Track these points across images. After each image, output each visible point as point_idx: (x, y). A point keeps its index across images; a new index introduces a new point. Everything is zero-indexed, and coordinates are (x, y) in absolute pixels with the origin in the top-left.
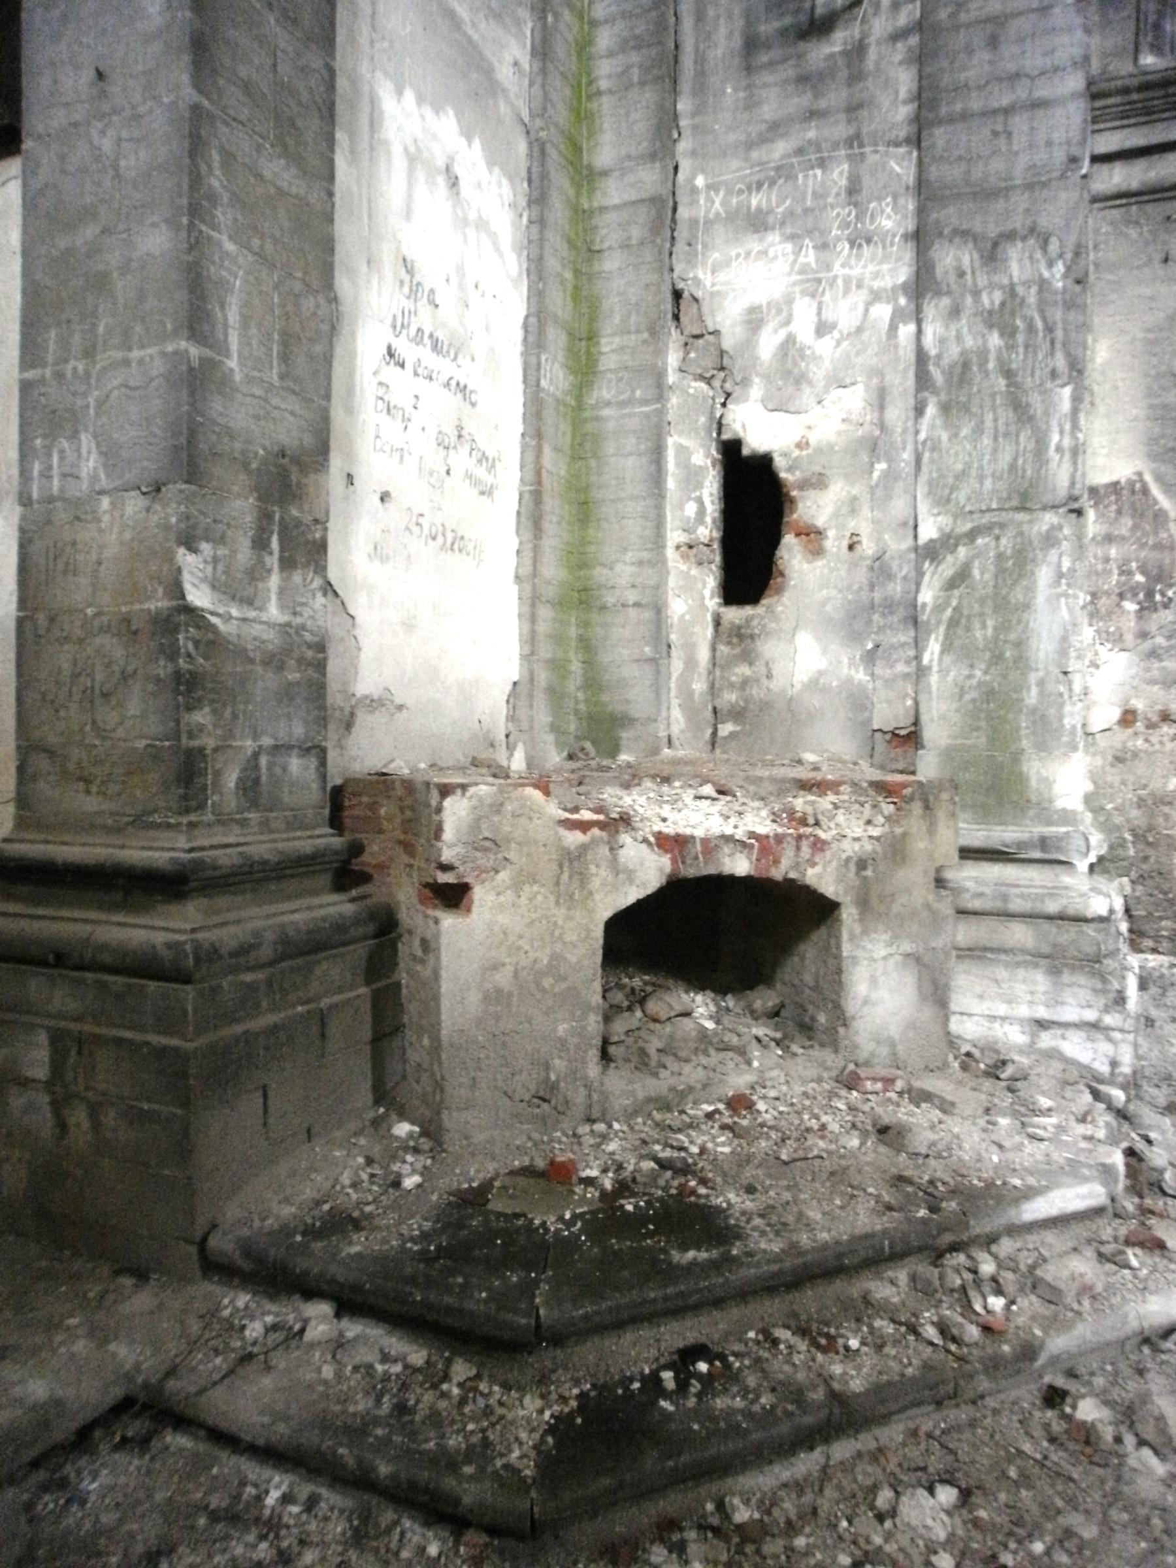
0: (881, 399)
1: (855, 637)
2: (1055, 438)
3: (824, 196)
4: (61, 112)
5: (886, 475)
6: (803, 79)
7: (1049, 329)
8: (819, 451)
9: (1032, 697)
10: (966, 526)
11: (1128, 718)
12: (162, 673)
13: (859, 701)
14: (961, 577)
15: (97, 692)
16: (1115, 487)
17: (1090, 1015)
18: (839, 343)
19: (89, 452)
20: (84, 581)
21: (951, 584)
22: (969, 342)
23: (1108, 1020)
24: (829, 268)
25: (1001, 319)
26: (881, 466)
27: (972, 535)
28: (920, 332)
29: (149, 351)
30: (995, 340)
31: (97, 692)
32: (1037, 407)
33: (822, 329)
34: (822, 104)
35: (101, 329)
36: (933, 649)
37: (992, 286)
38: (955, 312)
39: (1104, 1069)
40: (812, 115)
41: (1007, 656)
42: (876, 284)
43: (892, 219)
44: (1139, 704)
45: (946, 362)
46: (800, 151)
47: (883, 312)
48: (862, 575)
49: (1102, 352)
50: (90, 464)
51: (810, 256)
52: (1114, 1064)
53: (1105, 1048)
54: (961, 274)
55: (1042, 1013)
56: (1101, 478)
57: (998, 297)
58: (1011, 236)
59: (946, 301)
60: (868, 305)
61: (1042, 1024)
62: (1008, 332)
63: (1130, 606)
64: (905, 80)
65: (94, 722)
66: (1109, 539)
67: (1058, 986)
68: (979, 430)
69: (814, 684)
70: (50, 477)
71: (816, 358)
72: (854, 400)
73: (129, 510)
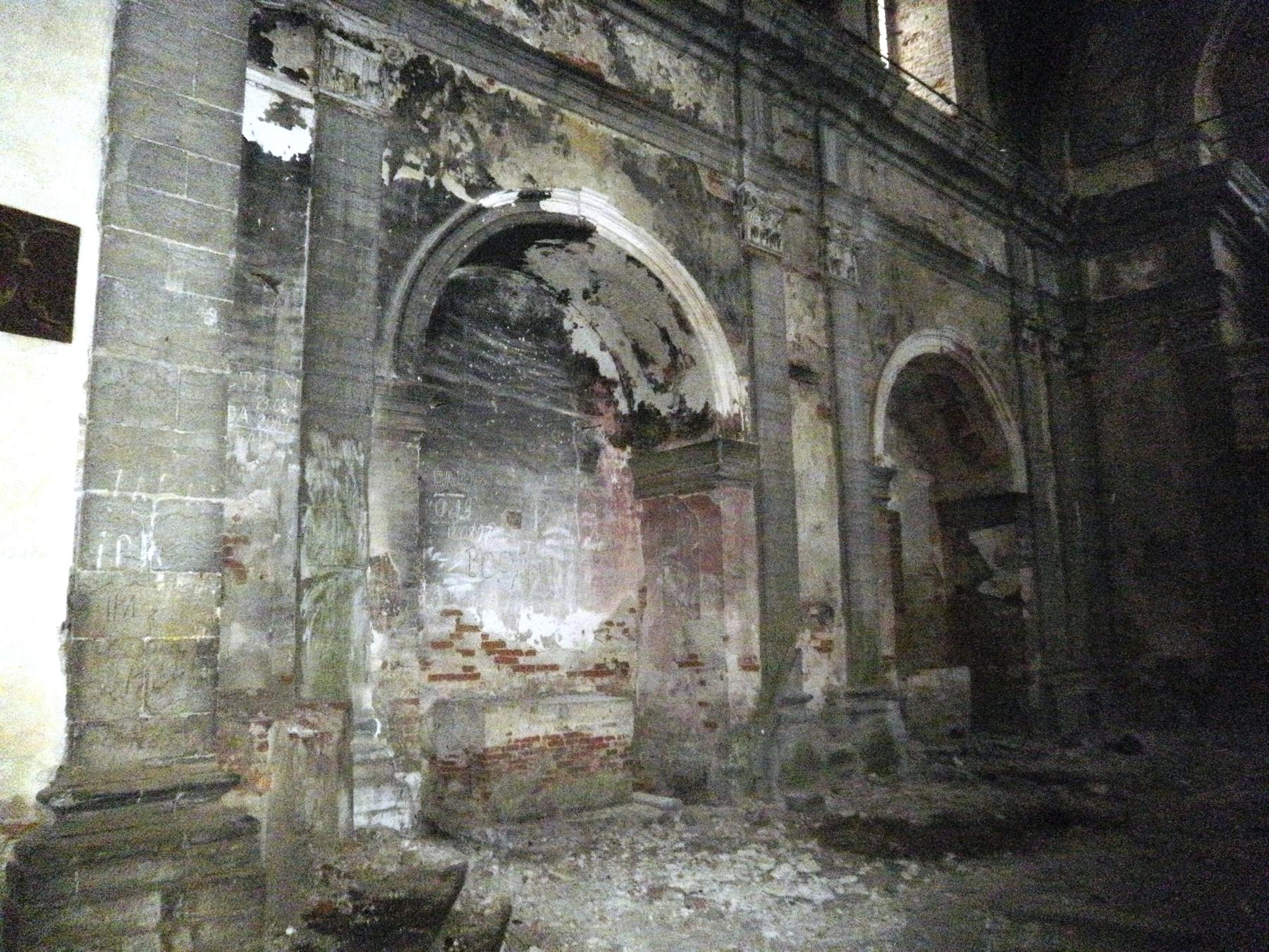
0: (279, 500)
1: (263, 627)
2: (361, 534)
3: (253, 388)
4: (133, 348)
5: (280, 541)
6: (245, 323)
7: (358, 484)
8: (247, 523)
9: (352, 656)
10: (322, 573)
11: (384, 665)
12: (204, 675)
13: (263, 660)
14: (321, 597)
15: (151, 686)
16: (378, 558)
17: (393, 803)
18: (258, 467)
19: (149, 546)
20: (143, 621)
21: (317, 601)
22: (326, 482)
23: (399, 804)
24: (255, 425)
25: (339, 473)
26: (277, 536)
27: (326, 577)
28: (303, 471)
29: (200, 499)
30: (336, 483)
31: (151, 686)
32: (353, 520)
33: (251, 457)
34: (254, 339)
35: (162, 479)
36: (307, 633)
37: (336, 458)
38: (320, 467)
39: (398, 827)
40: (248, 343)
41: (341, 636)
42: (278, 441)
43: (288, 409)
44: (389, 659)
45: (315, 489)
46: (241, 360)
47: (281, 455)
48: (267, 594)
49: (373, 497)
50: (149, 553)
51: (245, 416)
52: (402, 825)
53: (398, 817)
54: (322, 449)
55: (373, 807)
56: (373, 555)
57: (338, 464)
58: (344, 437)
59: (316, 461)
60: (274, 450)
61: (374, 813)
62: (342, 481)
63: (385, 614)
64: (297, 345)
65: (146, 705)
66: (377, 582)
67: (380, 793)
68: (329, 527)
69: (242, 652)
70: (114, 557)
71: (247, 473)
72: (264, 497)
73: (180, 582)
